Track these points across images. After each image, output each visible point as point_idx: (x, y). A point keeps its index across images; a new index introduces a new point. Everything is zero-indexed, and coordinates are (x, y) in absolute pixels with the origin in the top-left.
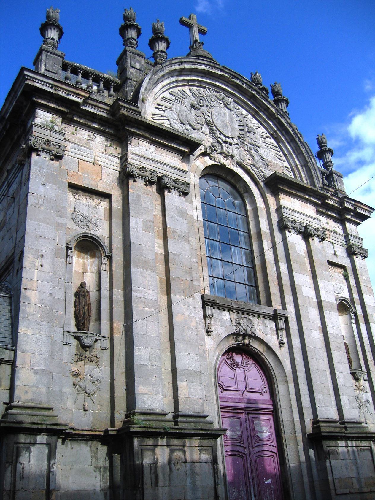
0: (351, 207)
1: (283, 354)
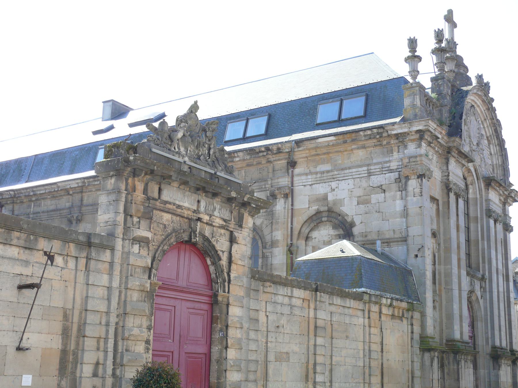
0: (513, 196)
1: (481, 302)
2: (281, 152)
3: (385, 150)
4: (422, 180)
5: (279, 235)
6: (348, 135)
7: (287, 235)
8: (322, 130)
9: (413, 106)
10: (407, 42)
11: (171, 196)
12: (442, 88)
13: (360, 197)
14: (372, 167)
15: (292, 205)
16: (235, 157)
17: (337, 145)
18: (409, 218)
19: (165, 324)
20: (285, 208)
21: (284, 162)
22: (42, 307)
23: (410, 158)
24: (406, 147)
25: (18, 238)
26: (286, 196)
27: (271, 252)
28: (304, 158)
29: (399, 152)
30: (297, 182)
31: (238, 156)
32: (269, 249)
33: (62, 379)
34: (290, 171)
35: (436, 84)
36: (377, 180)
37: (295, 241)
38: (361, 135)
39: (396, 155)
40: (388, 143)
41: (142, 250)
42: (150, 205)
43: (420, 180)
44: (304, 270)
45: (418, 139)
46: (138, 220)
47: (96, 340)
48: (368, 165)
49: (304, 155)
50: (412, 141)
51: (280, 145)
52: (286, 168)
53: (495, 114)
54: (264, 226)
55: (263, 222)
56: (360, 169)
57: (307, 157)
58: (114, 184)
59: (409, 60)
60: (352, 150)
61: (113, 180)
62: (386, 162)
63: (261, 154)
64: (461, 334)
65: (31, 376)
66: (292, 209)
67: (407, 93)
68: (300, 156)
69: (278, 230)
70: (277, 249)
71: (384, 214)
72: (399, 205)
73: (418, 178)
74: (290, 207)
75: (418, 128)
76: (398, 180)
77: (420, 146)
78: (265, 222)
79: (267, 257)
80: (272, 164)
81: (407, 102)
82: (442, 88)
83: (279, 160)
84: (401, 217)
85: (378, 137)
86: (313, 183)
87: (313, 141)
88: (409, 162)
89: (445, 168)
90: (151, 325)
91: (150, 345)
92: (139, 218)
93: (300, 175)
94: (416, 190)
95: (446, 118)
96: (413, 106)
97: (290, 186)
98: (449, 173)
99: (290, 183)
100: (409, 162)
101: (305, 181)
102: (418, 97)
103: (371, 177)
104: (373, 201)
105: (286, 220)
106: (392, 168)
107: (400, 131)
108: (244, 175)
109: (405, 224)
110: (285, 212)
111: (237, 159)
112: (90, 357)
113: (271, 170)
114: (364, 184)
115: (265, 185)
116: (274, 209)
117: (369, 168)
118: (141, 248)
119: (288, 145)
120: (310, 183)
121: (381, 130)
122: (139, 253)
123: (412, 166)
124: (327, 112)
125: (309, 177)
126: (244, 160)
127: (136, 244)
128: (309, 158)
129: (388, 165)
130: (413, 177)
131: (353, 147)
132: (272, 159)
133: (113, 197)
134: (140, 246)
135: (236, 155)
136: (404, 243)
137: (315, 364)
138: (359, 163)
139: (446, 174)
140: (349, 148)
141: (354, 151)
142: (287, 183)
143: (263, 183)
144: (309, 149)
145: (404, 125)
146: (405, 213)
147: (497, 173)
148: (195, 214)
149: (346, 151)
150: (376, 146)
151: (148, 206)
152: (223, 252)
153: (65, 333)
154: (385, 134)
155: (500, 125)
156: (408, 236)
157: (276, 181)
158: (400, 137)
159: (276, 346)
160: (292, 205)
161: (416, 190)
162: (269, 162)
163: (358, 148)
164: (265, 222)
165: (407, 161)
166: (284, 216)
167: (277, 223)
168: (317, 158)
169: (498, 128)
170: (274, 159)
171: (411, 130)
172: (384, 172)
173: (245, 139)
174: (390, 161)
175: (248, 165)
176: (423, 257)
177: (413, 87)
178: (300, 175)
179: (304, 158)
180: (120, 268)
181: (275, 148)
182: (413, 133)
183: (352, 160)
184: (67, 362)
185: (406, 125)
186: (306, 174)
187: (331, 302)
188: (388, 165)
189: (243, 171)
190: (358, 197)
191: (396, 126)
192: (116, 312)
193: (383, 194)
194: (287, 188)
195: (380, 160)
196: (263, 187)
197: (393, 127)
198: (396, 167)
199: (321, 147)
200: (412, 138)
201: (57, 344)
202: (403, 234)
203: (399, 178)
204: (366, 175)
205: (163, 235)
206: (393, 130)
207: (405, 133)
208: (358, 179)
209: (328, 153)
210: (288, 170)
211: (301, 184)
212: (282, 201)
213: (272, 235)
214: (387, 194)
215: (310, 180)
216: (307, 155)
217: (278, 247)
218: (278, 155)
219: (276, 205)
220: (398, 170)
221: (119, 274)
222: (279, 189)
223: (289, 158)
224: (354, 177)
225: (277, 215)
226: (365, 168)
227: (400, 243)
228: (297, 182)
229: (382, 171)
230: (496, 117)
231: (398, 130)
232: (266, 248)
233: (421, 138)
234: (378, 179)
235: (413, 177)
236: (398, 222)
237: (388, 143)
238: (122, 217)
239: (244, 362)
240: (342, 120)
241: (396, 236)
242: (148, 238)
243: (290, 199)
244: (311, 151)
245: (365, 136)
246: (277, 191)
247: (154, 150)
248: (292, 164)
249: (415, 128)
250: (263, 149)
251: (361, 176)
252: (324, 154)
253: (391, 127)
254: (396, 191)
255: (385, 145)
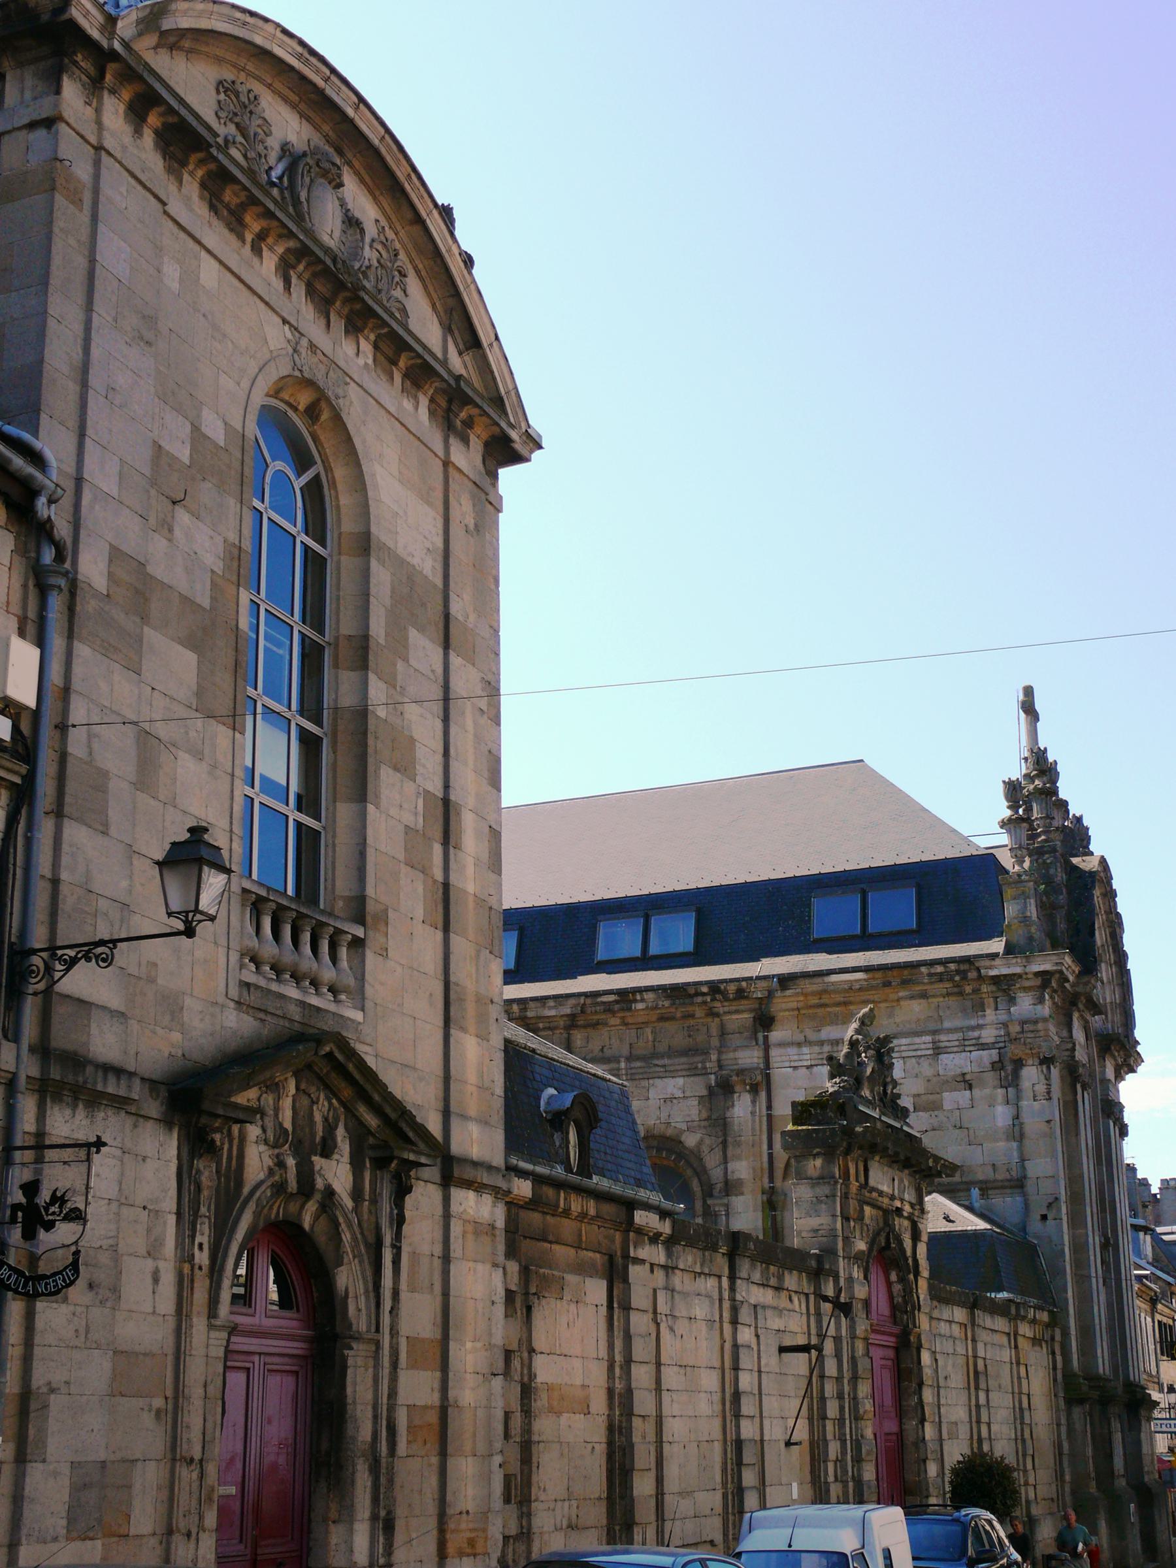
2: (747, 998)
3: (968, 1004)
4: (1049, 1068)
5: (741, 1169)
6: (895, 972)
7: (762, 1169)
8: (830, 953)
9: (1025, 920)
10: (1000, 790)
12: (1052, 871)
13: (919, 1095)
14: (943, 1037)
15: (769, 1107)
16: (635, 1001)
17: (872, 988)
18: (1026, 1142)
20: (753, 1113)
21: (747, 1017)
23: (1023, 1023)
24: (1012, 1001)
26: (754, 1089)
27: (727, 1206)
28: (793, 1010)
29: (996, 1009)
30: (779, 1059)
31: (643, 1000)
32: (717, 1198)
34: (760, 1035)
35: (1040, 861)
36: (953, 1063)
37: (778, 1183)
38: (922, 973)
39: (990, 1015)
40: (976, 991)
43: (1044, 1067)
45: (1039, 987)
48: (934, 1032)
49: (794, 1005)
50: (1025, 989)
51: (744, 984)
53: (1115, 903)
54: (705, 1149)
55: (702, 1140)
56: (917, 1040)
57: (798, 1009)
58: (822, 1167)
59: (1012, 826)
60: (898, 1000)
61: (819, 1162)
62: (973, 1028)
63: (699, 999)
64: (890, 1334)
66: (770, 1117)
67: (1008, 893)
68: (784, 1006)
69: (738, 1158)
70: (741, 1198)
71: (971, 1131)
72: (1002, 1115)
73: (1041, 1063)
74: (764, 1112)
75: (1042, 968)
76: (997, 1066)
77: (1041, 1001)
79: (716, 1216)
80: (717, 1020)
81: (1011, 910)
82: (1052, 871)
83: (737, 1012)
84: (1008, 1139)
85: (957, 978)
86: (813, 1063)
87: (819, 980)
88: (1023, 1032)
89: (1065, 1033)
93: (782, 1045)
94: (1037, 1088)
95: (1062, 932)
96: (1025, 920)
97: (762, 1066)
98: (1074, 1044)
99: (761, 1060)
100: (1023, 1032)
101: (796, 1057)
102: (1032, 901)
103: (941, 1057)
104: (947, 1106)
105: (757, 1138)
106: (982, 1041)
107: (1005, 971)
108: (650, 1038)
109: (1015, 1154)
110: (754, 1121)
111: (640, 1006)
113: (714, 1031)
114: (926, 1069)
115: (703, 1062)
116: (728, 1114)
117: (937, 1037)
119: (763, 984)
120: (808, 1063)
121: (963, 967)
123: (1029, 1040)
124: (827, 915)
125: (805, 1050)
126: (656, 1008)
128: (802, 1012)
129: (976, 1034)
130: (1030, 1062)
131: (901, 994)
132: (721, 1010)
133: (825, 1190)
135: (638, 997)
136: (1019, 1190)
138: (914, 1026)
139: (1070, 1046)
140: (893, 996)
141: (902, 1003)
142: (756, 1060)
143: (699, 1058)
144: (806, 995)
145: (1014, 961)
146: (1017, 1132)
147: (1113, 1022)
149: (886, 1001)
150: (948, 994)
154: (972, 975)
155: (1121, 924)
156: (1025, 1177)
157: (731, 1055)
158: (1005, 986)
160: (769, 1107)
161: (1037, 1088)
162: (712, 1014)
163: (912, 997)
164: (708, 1141)
165: (1018, 1029)
166: (753, 1129)
167: (738, 1144)
168: (820, 1011)
169: (1118, 930)
170: (726, 1009)
171: (1028, 970)
172: (967, 1049)
173: (645, 962)
174: (980, 1027)
175: (662, 1019)
176: (1058, 1219)
177: (1022, 882)
178: (782, 1045)
179: (793, 1010)
181: (732, 988)
182: (1030, 976)
183: (897, 1020)
185: (1019, 960)
186: (799, 1045)
188: (976, 1034)
189: (648, 1031)
190: (915, 1096)
191: (998, 962)
193: (968, 1092)
194: (758, 1072)
195: (958, 1023)
196: (700, 1065)
197: (993, 963)
198: (992, 1040)
199: (835, 992)
200: (1027, 984)
202: (1014, 1173)
203: (1000, 1061)
204: (930, 1052)
206: (991, 968)
207: (1014, 975)
208: (913, 1060)
209: (846, 1004)
210: (755, 1033)
211: (787, 1064)
212: (747, 1098)
213: (726, 1169)
214: (976, 1092)
215: (808, 1057)
216: (801, 1005)
217: (742, 1194)
218: (734, 1003)
219: (733, 1105)
220: (997, 1046)
222: (741, 1072)
223: (760, 1008)
224: (904, 1054)
225: (736, 1128)
226: (928, 1038)
227: (1008, 1191)
228: (779, 1059)
229: (963, 1047)
230: (1115, 907)
231: (1000, 969)
232: (711, 1196)
233: (1045, 985)
234: (956, 1061)
235: (1030, 1062)
236: (1003, 1151)
237: (976, 991)
240: (871, 935)
241: (1000, 1177)
243: (763, 1094)
244: (810, 998)
245: (930, 975)
246: (735, 1078)
247: (861, 1108)
248: (764, 1021)
249: (1036, 968)
250: (705, 989)
251: (919, 1053)
252: (838, 1004)
253: (987, 963)
254: (995, 1087)
255: (969, 994)
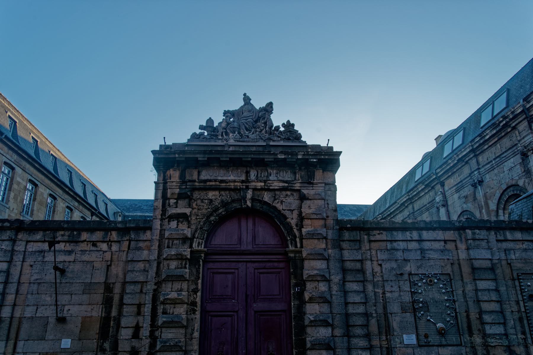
11: (211, 174)
19: (227, 286)
22: (83, 284)
25: (62, 235)
33: (104, 341)
41: (180, 225)
42: (188, 187)
44: (517, 212)
46: (175, 201)
47: (136, 306)
52: (528, 126)
54: (527, 184)
55: (525, 181)
65: (70, 340)
78: (527, 181)
90: (197, 288)
91: (196, 307)
92: (175, 199)
112: (128, 321)
113: (518, 134)
118: (180, 223)
122: (177, 227)
127: (173, 221)
134: (178, 222)
137: (481, 313)
148: (244, 184)
151: (186, 188)
152: (292, 211)
153: (108, 303)
159: (400, 296)
180: (158, 244)
184: (108, 328)
187: (502, 238)
192: (154, 280)
201: (97, 312)
205: (209, 208)
221: (157, 248)
238: (160, 202)
239: (338, 316)
242: (185, 214)
